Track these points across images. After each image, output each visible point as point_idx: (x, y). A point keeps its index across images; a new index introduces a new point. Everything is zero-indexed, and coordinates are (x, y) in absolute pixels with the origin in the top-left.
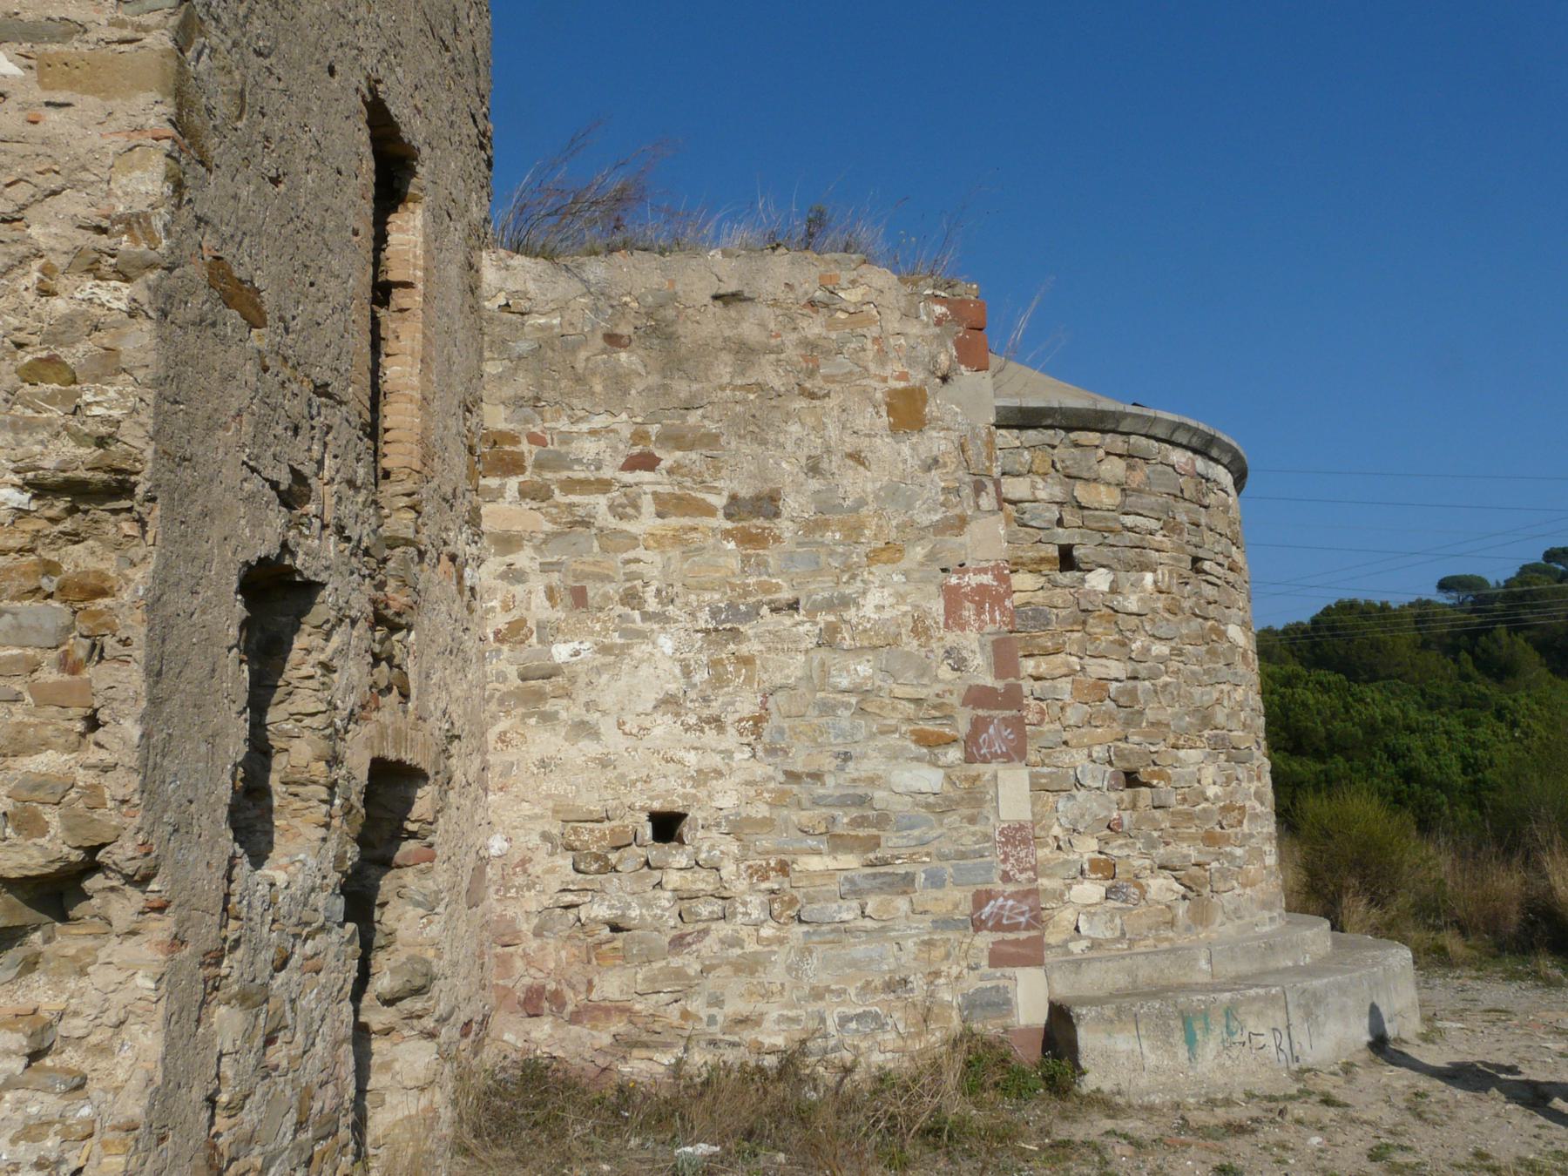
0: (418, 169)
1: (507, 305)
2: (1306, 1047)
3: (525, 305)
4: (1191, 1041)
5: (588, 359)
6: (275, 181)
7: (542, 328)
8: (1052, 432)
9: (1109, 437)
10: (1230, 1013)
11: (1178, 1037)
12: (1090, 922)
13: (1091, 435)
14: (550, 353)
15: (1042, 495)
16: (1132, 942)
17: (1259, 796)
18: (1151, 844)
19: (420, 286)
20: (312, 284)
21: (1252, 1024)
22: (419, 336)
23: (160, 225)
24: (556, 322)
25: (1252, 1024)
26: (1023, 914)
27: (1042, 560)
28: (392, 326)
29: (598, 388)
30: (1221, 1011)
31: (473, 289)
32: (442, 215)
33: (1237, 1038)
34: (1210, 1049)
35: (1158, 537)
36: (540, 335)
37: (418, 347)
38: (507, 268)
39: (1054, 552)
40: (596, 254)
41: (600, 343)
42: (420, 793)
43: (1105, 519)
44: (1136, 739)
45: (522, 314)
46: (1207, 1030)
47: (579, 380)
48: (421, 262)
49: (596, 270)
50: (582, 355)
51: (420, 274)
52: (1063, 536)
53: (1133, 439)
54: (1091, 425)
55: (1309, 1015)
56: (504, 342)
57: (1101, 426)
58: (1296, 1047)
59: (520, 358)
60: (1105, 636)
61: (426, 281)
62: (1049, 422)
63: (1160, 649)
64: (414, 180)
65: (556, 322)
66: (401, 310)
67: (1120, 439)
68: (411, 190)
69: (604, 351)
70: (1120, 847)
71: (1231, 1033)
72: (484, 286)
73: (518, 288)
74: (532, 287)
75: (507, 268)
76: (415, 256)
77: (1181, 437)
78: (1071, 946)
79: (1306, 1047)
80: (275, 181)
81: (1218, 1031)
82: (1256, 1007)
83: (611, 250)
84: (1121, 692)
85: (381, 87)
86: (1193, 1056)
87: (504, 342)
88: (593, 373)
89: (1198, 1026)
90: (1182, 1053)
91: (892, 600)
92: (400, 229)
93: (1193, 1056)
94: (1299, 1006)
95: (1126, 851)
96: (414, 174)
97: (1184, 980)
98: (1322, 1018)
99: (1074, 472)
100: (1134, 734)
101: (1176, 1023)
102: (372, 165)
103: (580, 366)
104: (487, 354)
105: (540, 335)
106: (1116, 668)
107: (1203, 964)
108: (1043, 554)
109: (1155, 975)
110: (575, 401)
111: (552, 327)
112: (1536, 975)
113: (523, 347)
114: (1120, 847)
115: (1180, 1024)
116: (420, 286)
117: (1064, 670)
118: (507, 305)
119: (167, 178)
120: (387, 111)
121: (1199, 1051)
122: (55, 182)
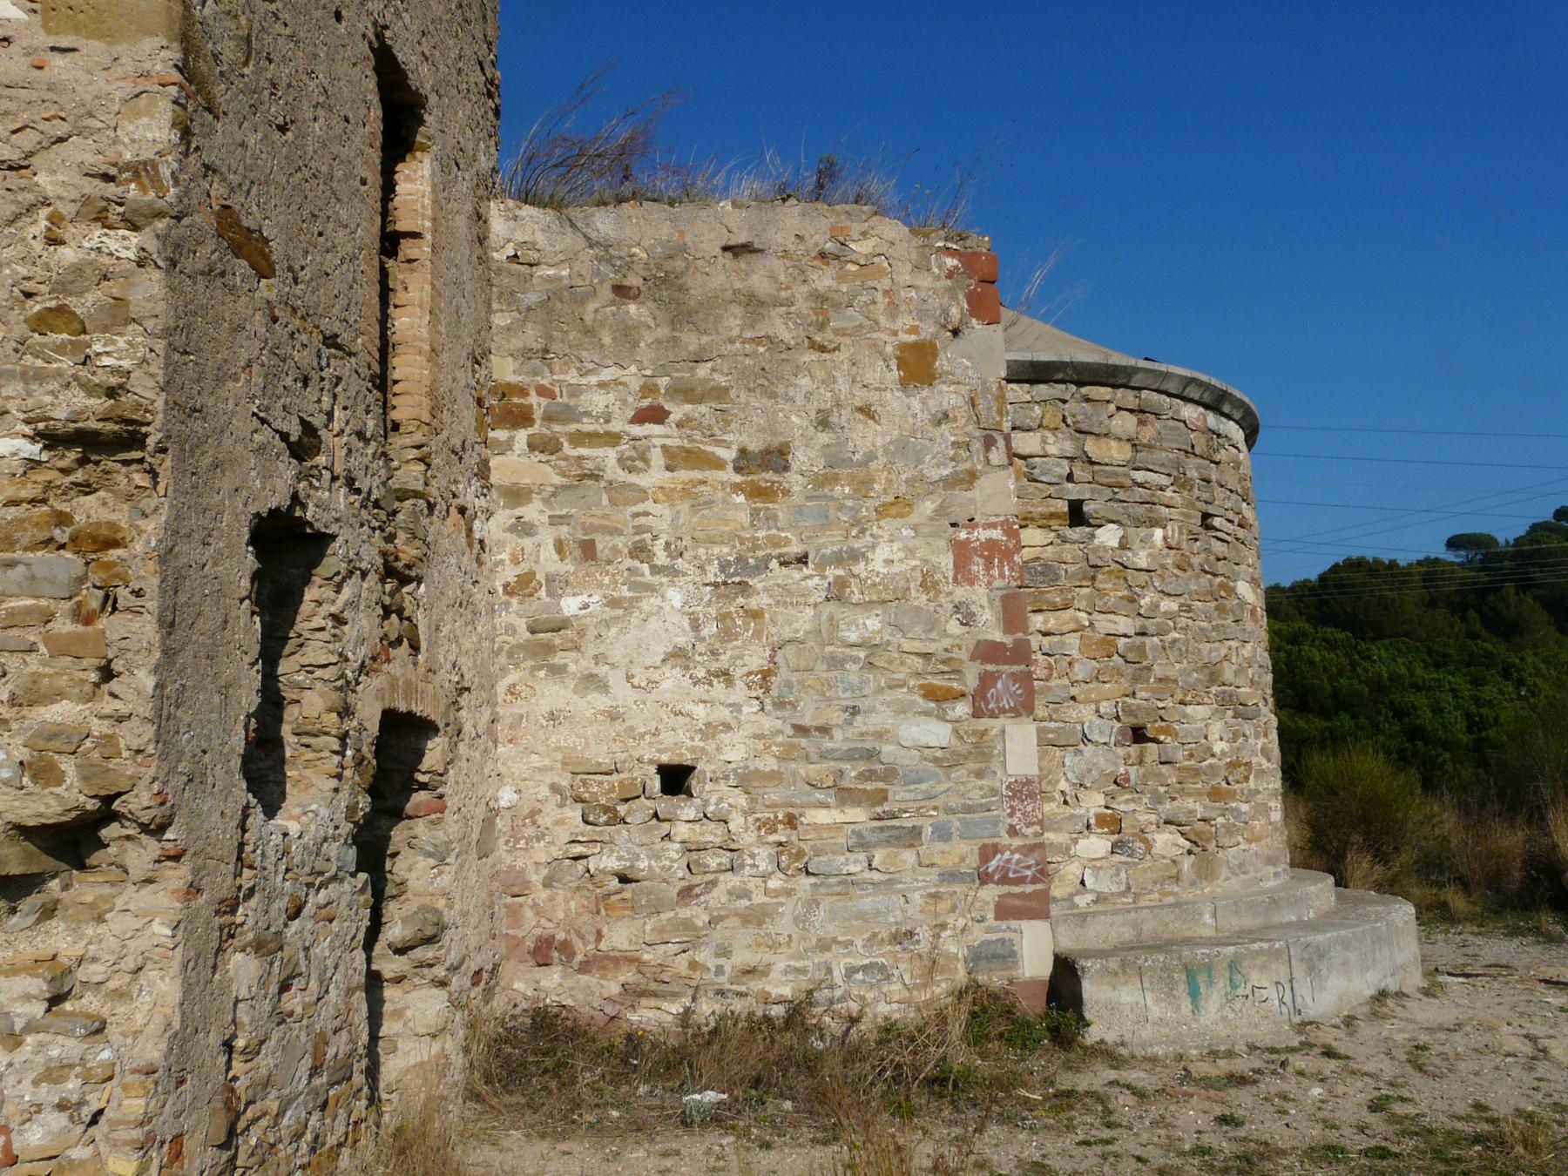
0: (426, 117)
1: (516, 256)
2: (1308, 999)
3: (533, 256)
4: (1194, 994)
5: (596, 311)
6: (283, 129)
7: (550, 279)
8: (1063, 387)
9: (1120, 392)
10: (1233, 966)
11: (1182, 989)
12: (1096, 877)
13: (1103, 390)
14: (559, 305)
15: (1052, 450)
16: (1137, 896)
17: (1265, 752)
18: (1158, 799)
19: (428, 237)
20: (320, 234)
21: (1255, 978)
22: (428, 287)
23: (168, 173)
24: (565, 273)
25: (1255, 978)
26: (1029, 867)
27: (1052, 516)
28: (401, 276)
29: (607, 340)
30: (1225, 965)
31: (481, 240)
32: (450, 165)
33: (1240, 991)
34: (1213, 1001)
35: (1169, 493)
36: (549, 286)
37: (427, 298)
38: (516, 218)
39: (1063, 507)
40: (605, 204)
41: (606, 293)
42: (430, 744)
43: (1116, 474)
44: (1144, 694)
45: (531, 265)
46: (1211, 983)
47: (588, 332)
48: (429, 212)
49: (604, 222)
50: (591, 306)
51: (428, 224)
52: (1073, 491)
53: (1144, 394)
54: (1103, 380)
55: (1312, 969)
56: (512, 293)
57: (1111, 381)
58: (1299, 1000)
59: (529, 309)
60: (1115, 592)
61: (435, 231)
62: (1060, 376)
63: (1169, 605)
64: (422, 129)
65: (565, 273)
66: (410, 261)
67: (1131, 393)
68: (419, 138)
69: (613, 303)
70: (1127, 802)
71: (1234, 987)
72: (492, 237)
73: (527, 238)
74: (540, 238)
75: (516, 218)
76: (423, 206)
77: (1194, 393)
78: (1077, 899)
79: (1308, 999)
80: (283, 129)
81: (1222, 984)
82: (1260, 960)
83: (620, 200)
84: (1129, 648)
85: (388, 34)
86: (1196, 1008)
87: (512, 293)
88: (602, 325)
89: (1201, 979)
90: (1186, 1006)
91: (901, 555)
92: (408, 179)
93: (1196, 1008)
94: (1302, 960)
95: (1132, 806)
96: (422, 122)
97: (1188, 934)
98: (1324, 972)
99: (1084, 427)
100: (1142, 690)
101: (1180, 977)
102: (380, 113)
103: (589, 318)
104: (495, 306)
105: (549, 286)
106: (1124, 624)
107: (1208, 918)
108: (1052, 509)
109: (1160, 929)
110: (584, 354)
111: (560, 279)
112: (1537, 931)
113: (532, 298)
114: (1127, 802)
115: (1184, 977)
116: (428, 237)
117: (1072, 626)
118: (516, 256)
119: (174, 125)
120: (394, 58)
121: (1202, 1003)
122: (61, 129)
